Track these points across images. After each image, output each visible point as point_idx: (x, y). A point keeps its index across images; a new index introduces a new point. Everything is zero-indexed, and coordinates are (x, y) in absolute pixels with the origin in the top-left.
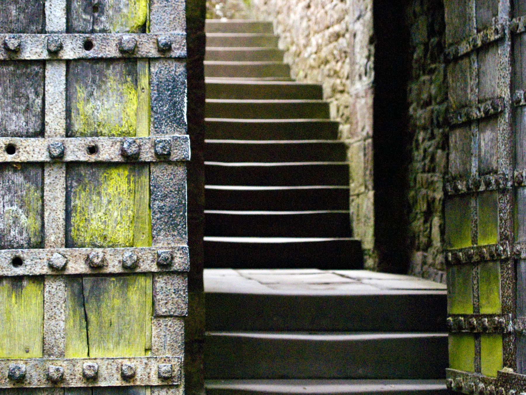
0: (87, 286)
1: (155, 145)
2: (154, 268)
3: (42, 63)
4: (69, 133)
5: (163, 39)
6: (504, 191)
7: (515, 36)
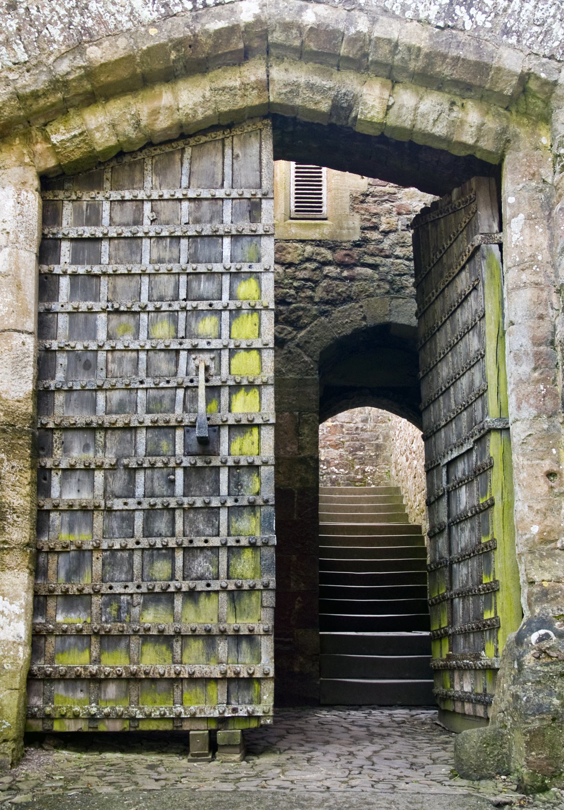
0: (236, 595)
2: (262, 588)
4: (229, 535)
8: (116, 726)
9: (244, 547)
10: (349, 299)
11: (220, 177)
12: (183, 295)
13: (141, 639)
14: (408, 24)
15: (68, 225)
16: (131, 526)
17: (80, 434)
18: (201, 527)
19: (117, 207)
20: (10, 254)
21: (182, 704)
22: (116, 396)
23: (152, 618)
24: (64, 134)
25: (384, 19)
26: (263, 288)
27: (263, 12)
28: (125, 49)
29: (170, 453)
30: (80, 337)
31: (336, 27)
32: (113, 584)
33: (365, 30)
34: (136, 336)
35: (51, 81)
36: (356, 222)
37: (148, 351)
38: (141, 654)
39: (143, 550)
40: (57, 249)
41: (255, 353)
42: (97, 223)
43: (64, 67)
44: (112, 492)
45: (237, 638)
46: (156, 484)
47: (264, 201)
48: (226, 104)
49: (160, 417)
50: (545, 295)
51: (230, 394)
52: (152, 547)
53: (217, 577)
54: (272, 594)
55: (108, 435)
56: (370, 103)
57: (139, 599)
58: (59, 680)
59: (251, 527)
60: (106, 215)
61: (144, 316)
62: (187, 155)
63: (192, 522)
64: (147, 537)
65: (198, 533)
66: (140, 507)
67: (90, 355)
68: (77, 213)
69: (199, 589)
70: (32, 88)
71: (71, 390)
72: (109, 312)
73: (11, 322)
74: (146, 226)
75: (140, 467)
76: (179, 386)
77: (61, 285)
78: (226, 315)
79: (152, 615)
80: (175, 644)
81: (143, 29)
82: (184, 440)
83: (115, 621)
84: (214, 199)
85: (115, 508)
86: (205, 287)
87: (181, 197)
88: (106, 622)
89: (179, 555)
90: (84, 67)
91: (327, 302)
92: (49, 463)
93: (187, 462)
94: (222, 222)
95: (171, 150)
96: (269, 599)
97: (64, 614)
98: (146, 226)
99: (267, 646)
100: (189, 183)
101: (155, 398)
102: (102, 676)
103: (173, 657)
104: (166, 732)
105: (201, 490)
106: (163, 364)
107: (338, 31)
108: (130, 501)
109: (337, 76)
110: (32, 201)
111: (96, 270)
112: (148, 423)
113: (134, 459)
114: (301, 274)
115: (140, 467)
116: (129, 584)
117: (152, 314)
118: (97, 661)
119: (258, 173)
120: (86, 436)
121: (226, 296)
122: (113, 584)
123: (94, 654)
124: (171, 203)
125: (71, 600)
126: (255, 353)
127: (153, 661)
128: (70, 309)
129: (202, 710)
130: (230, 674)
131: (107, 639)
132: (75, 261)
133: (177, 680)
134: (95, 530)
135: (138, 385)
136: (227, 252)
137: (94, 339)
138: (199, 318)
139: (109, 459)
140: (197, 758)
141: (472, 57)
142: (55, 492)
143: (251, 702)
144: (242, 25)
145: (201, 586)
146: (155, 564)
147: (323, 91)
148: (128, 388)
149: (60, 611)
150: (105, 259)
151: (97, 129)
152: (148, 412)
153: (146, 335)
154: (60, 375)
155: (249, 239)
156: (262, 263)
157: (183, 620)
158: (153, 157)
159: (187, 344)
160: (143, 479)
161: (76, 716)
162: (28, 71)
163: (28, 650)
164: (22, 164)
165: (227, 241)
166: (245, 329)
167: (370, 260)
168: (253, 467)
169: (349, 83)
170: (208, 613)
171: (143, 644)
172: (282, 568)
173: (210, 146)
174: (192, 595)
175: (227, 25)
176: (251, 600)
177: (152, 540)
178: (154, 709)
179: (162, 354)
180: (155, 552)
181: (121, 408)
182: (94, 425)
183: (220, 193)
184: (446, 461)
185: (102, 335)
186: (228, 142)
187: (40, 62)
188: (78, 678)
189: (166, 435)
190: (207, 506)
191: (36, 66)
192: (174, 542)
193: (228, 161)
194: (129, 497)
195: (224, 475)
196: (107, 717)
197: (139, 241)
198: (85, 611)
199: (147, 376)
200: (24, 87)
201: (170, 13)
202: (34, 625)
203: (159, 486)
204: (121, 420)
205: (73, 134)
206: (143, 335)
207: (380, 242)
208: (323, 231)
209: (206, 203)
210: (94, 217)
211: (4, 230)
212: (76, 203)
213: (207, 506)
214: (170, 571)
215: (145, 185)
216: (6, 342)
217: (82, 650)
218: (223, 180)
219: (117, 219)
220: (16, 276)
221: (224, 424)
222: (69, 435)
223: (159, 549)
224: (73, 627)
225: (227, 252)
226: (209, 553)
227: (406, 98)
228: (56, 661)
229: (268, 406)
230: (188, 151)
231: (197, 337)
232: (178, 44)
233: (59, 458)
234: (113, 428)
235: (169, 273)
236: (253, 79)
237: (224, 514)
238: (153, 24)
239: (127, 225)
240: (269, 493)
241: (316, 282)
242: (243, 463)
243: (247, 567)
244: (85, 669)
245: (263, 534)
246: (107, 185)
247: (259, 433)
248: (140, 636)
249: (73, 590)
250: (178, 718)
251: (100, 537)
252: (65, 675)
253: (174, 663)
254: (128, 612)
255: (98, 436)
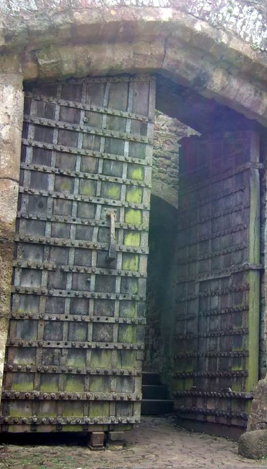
0: (122, 353)
1: (138, 320)
2: (137, 349)
3: (114, 300)
4: (120, 317)
5: (141, 296)
6: (195, 339)
7: (200, 297)
8: (48, 429)
9: (128, 324)
11: (125, 105)
12: (100, 171)
13: (66, 376)
14: (246, 44)
16: (63, 307)
17: (34, 247)
18: (104, 311)
19: (64, 110)
20: (10, 130)
21: (88, 416)
22: (58, 227)
23: (73, 363)
24: (47, 60)
26: (145, 175)
27: (174, 17)
28: (96, 19)
29: (88, 265)
30: (36, 187)
31: (211, 37)
32: (50, 341)
33: (226, 43)
34: (72, 192)
35: (50, 27)
37: (78, 201)
38: (65, 385)
39: (69, 322)
41: (139, 212)
42: (52, 117)
43: (59, 20)
44: (52, 285)
45: (122, 377)
46: (79, 282)
47: (149, 124)
51: (124, 234)
52: (75, 321)
53: (111, 341)
55: (52, 250)
56: (215, 82)
57: (65, 352)
58: (14, 401)
59: (131, 313)
60: (57, 113)
62: (108, 88)
63: (99, 307)
64: (72, 314)
65: (102, 314)
66: (69, 296)
67: (43, 199)
68: (40, 110)
69: (101, 347)
70: (39, 29)
71: (30, 219)
72: (56, 174)
73: (8, 173)
74: (82, 125)
77: (27, 152)
78: (124, 187)
79: (73, 362)
80: (86, 379)
81: (107, 9)
82: (97, 258)
83: (51, 365)
84: (121, 117)
85: (54, 295)
87: (103, 112)
88: (45, 364)
89: (91, 327)
90: (71, 24)
94: (125, 132)
95: (99, 82)
96: (140, 355)
97: (19, 359)
100: (108, 104)
101: (81, 231)
102: (42, 399)
103: (85, 388)
104: (78, 433)
105: (104, 288)
107: (212, 40)
108: (63, 291)
109: (202, 62)
112: (77, 245)
113: (68, 267)
116: (60, 342)
117: (82, 180)
119: (147, 107)
120: (38, 250)
121: (124, 176)
122: (50, 341)
123: (36, 384)
124: (96, 114)
126: (139, 212)
127: (73, 389)
128: (32, 168)
129: (101, 420)
130: (118, 399)
131: (44, 375)
132: (36, 139)
134: (40, 308)
135: (72, 222)
136: (126, 150)
137: (46, 188)
138: (109, 186)
140: (97, 448)
143: (128, 415)
144: (162, 22)
145: (102, 346)
146: (76, 331)
147: (192, 68)
148: (66, 223)
149: (16, 357)
150: (55, 141)
151: (67, 62)
152: (77, 238)
153: (77, 192)
155: (140, 144)
156: (146, 160)
157: (92, 366)
158: (88, 84)
159: (102, 201)
160: (71, 279)
161: (24, 423)
162: (36, 17)
165: (127, 144)
166: (134, 198)
168: (134, 278)
171: (67, 380)
172: (145, 337)
174: (97, 351)
175: (154, 20)
176: (130, 356)
177: (76, 316)
178: (73, 418)
179: (87, 205)
180: (76, 324)
182: (44, 243)
183: (125, 114)
184: (201, 280)
185: (51, 188)
187: (45, 14)
189: (87, 254)
191: (42, 15)
192: (89, 318)
194: (63, 289)
195: (118, 282)
197: (77, 134)
198: (32, 357)
199: (77, 217)
200: (33, 26)
201: (124, 4)
203: (81, 284)
204: (59, 241)
205: (52, 61)
206: (76, 191)
209: (117, 118)
210: (50, 114)
211: (6, 113)
212: (40, 102)
214: (85, 336)
215: (82, 100)
216: (6, 186)
217: (29, 382)
218: (127, 107)
219: (64, 117)
221: (121, 251)
222: (27, 248)
223: (79, 322)
224: (25, 367)
225: (126, 150)
226: (108, 326)
228: (12, 388)
229: (145, 244)
230: (109, 84)
231: (107, 197)
234: (55, 246)
236: (157, 53)
238: (113, 8)
239: (70, 122)
240: (143, 294)
242: (130, 275)
243: (129, 335)
244: (32, 393)
245: (139, 317)
246: (59, 95)
247: (139, 260)
248: (66, 374)
249: (26, 344)
250: (87, 424)
251: (43, 312)
252: (18, 397)
253: (85, 391)
254: (59, 359)
255: (45, 250)
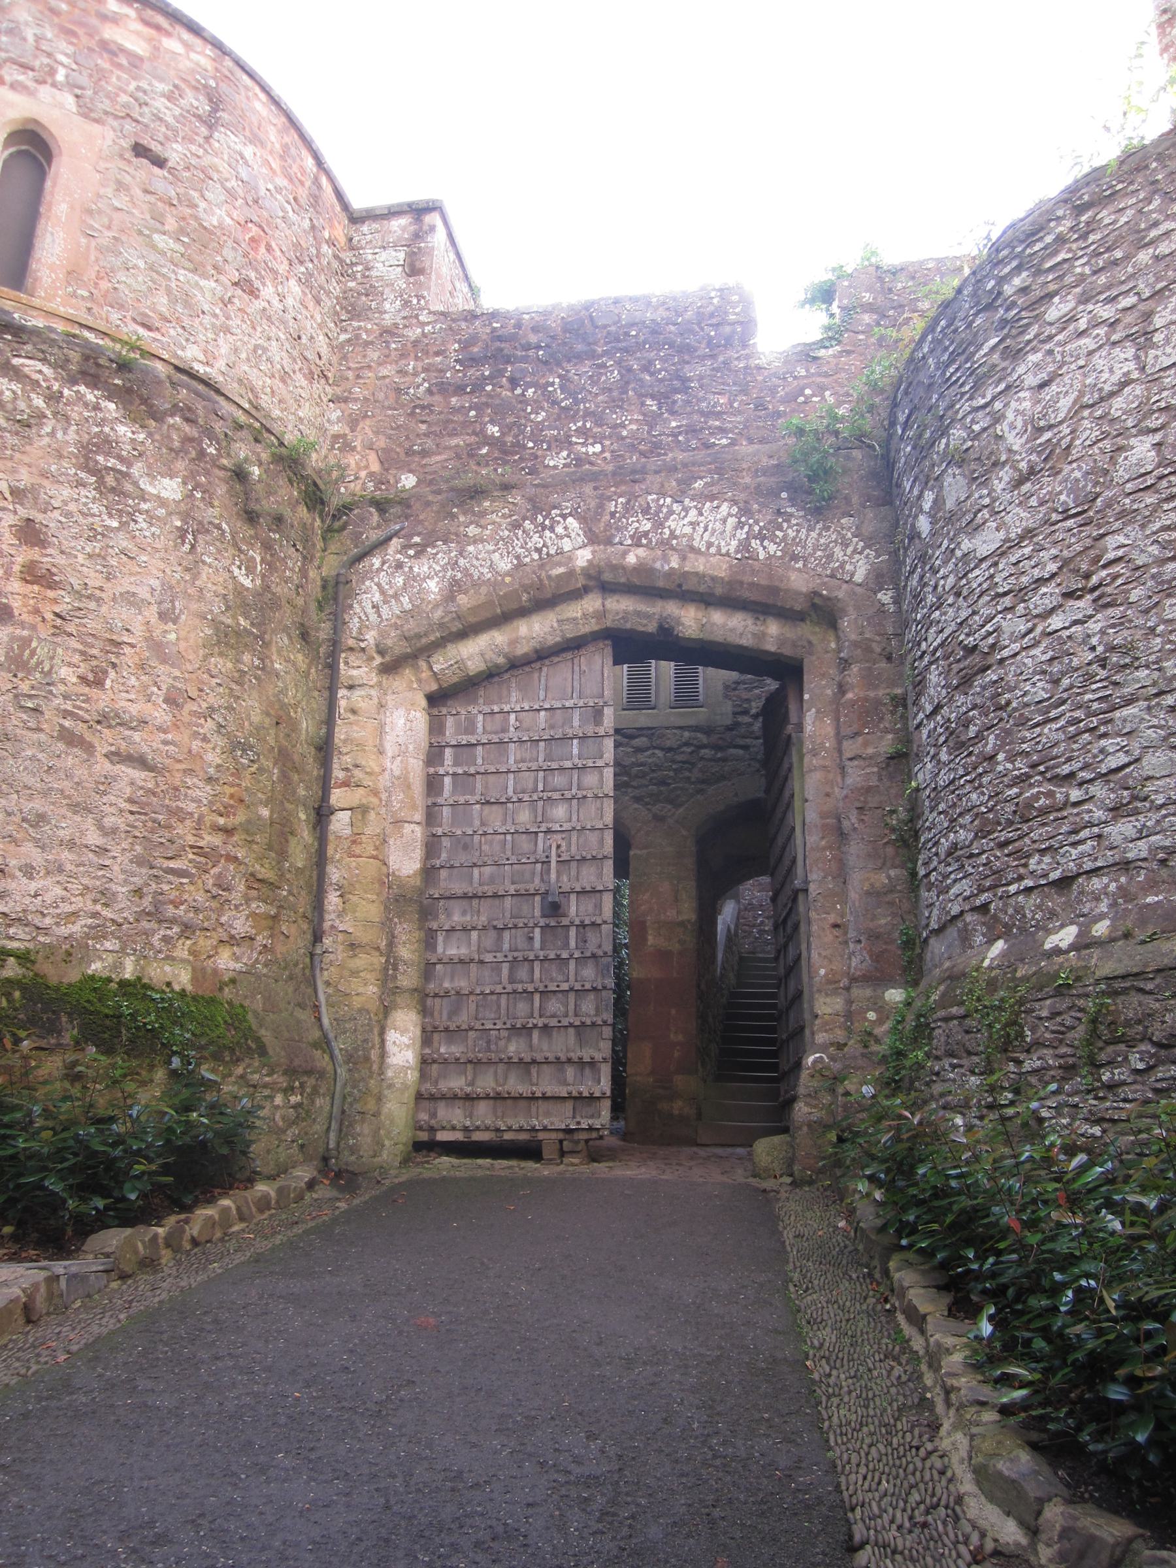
10: (723, 778)
12: (540, 787)
15: (451, 734)
19: (488, 718)
25: (691, 556)
36: (728, 707)
38: (506, 1078)
40: (441, 755)
45: (581, 1064)
48: (571, 632)
49: (521, 887)
50: (831, 776)
52: (515, 992)
54: (610, 1028)
60: (480, 725)
61: (510, 805)
65: (552, 980)
68: (458, 725)
71: (452, 867)
75: (506, 928)
76: (537, 862)
84: (564, 708)
86: (558, 780)
89: (537, 997)
91: (703, 782)
92: (435, 925)
93: (542, 922)
96: (607, 1032)
98: (512, 733)
99: (606, 1071)
106: (524, 843)
110: (420, 719)
111: (472, 770)
114: (679, 758)
115: (506, 928)
118: (472, 1084)
120: (465, 903)
125: (450, 1033)
127: (515, 1085)
130: (575, 1094)
133: (533, 1098)
136: (575, 751)
137: (471, 825)
139: (483, 919)
141: (764, 582)
142: (440, 949)
143: (592, 1117)
145: (553, 1022)
147: (648, 616)
150: (479, 761)
154: (444, 855)
161: (454, 1128)
163: (417, 1074)
164: (411, 689)
167: (741, 742)
169: (672, 609)
170: (562, 1045)
173: (562, 665)
177: (515, 986)
181: (492, 880)
186: (576, 661)
188: (455, 1097)
190: (558, 957)
193: (576, 677)
195: (573, 932)
196: (478, 1128)
202: (423, 1056)
203: (521, 943)
207: (751, 724)
208: (700, 715)
210: (470, 728)
213: (558, 957)
219: (488, 729)
220: (406, 778)
222: (452, 902)
225: (575, 751)
227: (718, 617)
230: (545, 669)
232: (526, 588)
233: (444, 921)
234: (484, 896)
235: (529, 770)
237: (572, 964)
238: (508, 574)
239: (496, 733)
241: (693, 764)
246: (481, 701)
249: (453, 1027)
